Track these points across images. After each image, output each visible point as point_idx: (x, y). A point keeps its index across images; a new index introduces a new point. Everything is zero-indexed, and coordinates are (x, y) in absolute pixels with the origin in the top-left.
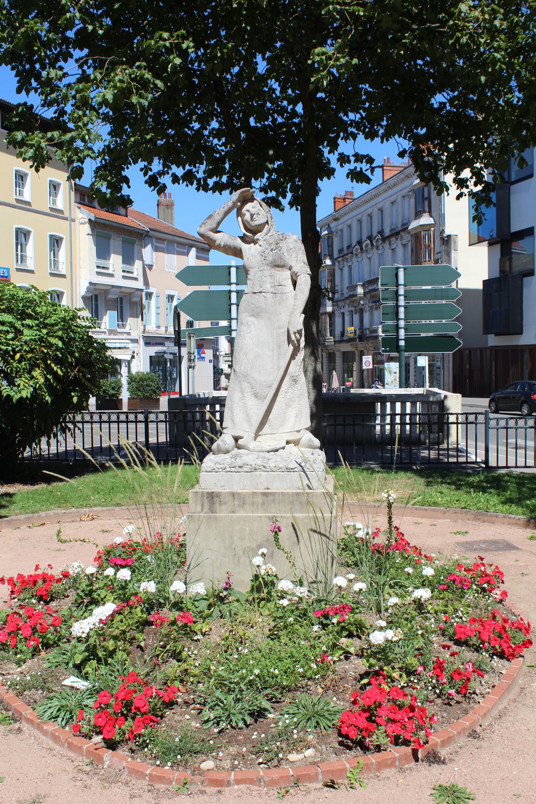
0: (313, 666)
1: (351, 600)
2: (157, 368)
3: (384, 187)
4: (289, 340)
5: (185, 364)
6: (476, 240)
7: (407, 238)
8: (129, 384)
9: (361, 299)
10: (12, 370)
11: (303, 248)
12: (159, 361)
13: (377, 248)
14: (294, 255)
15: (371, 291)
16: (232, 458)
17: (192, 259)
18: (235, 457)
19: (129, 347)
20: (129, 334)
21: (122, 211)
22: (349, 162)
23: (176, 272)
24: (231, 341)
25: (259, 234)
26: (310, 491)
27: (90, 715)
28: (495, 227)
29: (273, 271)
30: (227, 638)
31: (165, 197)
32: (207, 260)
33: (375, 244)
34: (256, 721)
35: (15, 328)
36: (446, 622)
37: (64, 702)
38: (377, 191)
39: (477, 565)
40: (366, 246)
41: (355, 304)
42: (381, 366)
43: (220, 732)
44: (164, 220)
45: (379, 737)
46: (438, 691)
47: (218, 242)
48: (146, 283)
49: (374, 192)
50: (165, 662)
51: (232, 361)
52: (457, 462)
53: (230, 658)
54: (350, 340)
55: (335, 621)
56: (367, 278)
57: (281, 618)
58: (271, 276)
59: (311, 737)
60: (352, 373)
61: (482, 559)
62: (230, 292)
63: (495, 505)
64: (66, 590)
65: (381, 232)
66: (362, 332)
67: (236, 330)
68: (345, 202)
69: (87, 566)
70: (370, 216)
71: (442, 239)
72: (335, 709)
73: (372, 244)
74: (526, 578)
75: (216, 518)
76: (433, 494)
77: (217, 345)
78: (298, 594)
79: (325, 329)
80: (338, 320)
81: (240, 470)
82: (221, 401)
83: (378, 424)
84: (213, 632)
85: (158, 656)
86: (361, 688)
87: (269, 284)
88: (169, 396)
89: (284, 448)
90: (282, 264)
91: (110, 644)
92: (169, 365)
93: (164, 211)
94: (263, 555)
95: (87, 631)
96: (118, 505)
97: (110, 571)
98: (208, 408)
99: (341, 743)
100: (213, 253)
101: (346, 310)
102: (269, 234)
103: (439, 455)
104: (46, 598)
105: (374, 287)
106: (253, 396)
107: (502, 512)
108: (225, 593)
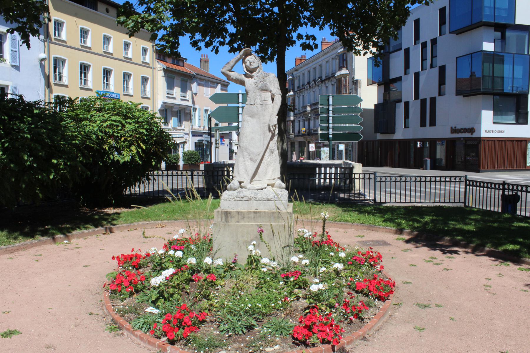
0: (280, 303)
1: (300, 269)
3: (322, 53)
4: (270, 130)
6: (371, 83)
7: (334, 81)
8: (183, 157)
9: (309, 113)
10: (120, 147)
13: (318, 86)
14: (273, 84)
17: (218, 90)
18: (239, 192)
19: (184, 136)
20: (183, 130)
21: (181, 64)
22: (302, 39)
24: (238, 134)
27: (160, 326)
28: (381, 76)
29: (261, 93)
30: (234, 288)
32: (227, 91)
34: (249, 331)
35: (122, 124)
36: (351, 281)
37: (146, 320)
39: (368, 252)
42: (319, 150)
43: (229, 336)
45: (314, 339)
46: (346, 317)
47: (232, 77)
48: (193, 103)
49: (317, 56)
50: (200, 300)
52: (359, 200)
53: (236, 298)
54: (303, 135)
55: (292, 279)
56: (312, 102)
57: (263, 278)
59: (278, 339)
61: (371, 248)
62: (238, 107)
63: (378, 222)
64: (148, 263)
65: (320, 77)
66: (309, 131)
69: (159, 250)
70: (315, 69)
71: (353, 82)
72: (291, 325)
73: (315, 84)
74: (394, 260)
76: (346, 216)
77: (231, 137)
78: (272, 265)
79: (290, 129)
80: (297, 124)
84: (227, 285)
85: (196, 297)
86: (305, 315)
89: (266, 188)
91: (171, 290)
94: (254, 245)
95: (159, 283)
96: (176, 219)
97: (171, 252)
99: (293, 343)
101: (301, 119)
103: (349, 196)
104: (137, 267)
105: (316, 107)
107: (382, 225)
108: (233, 265)
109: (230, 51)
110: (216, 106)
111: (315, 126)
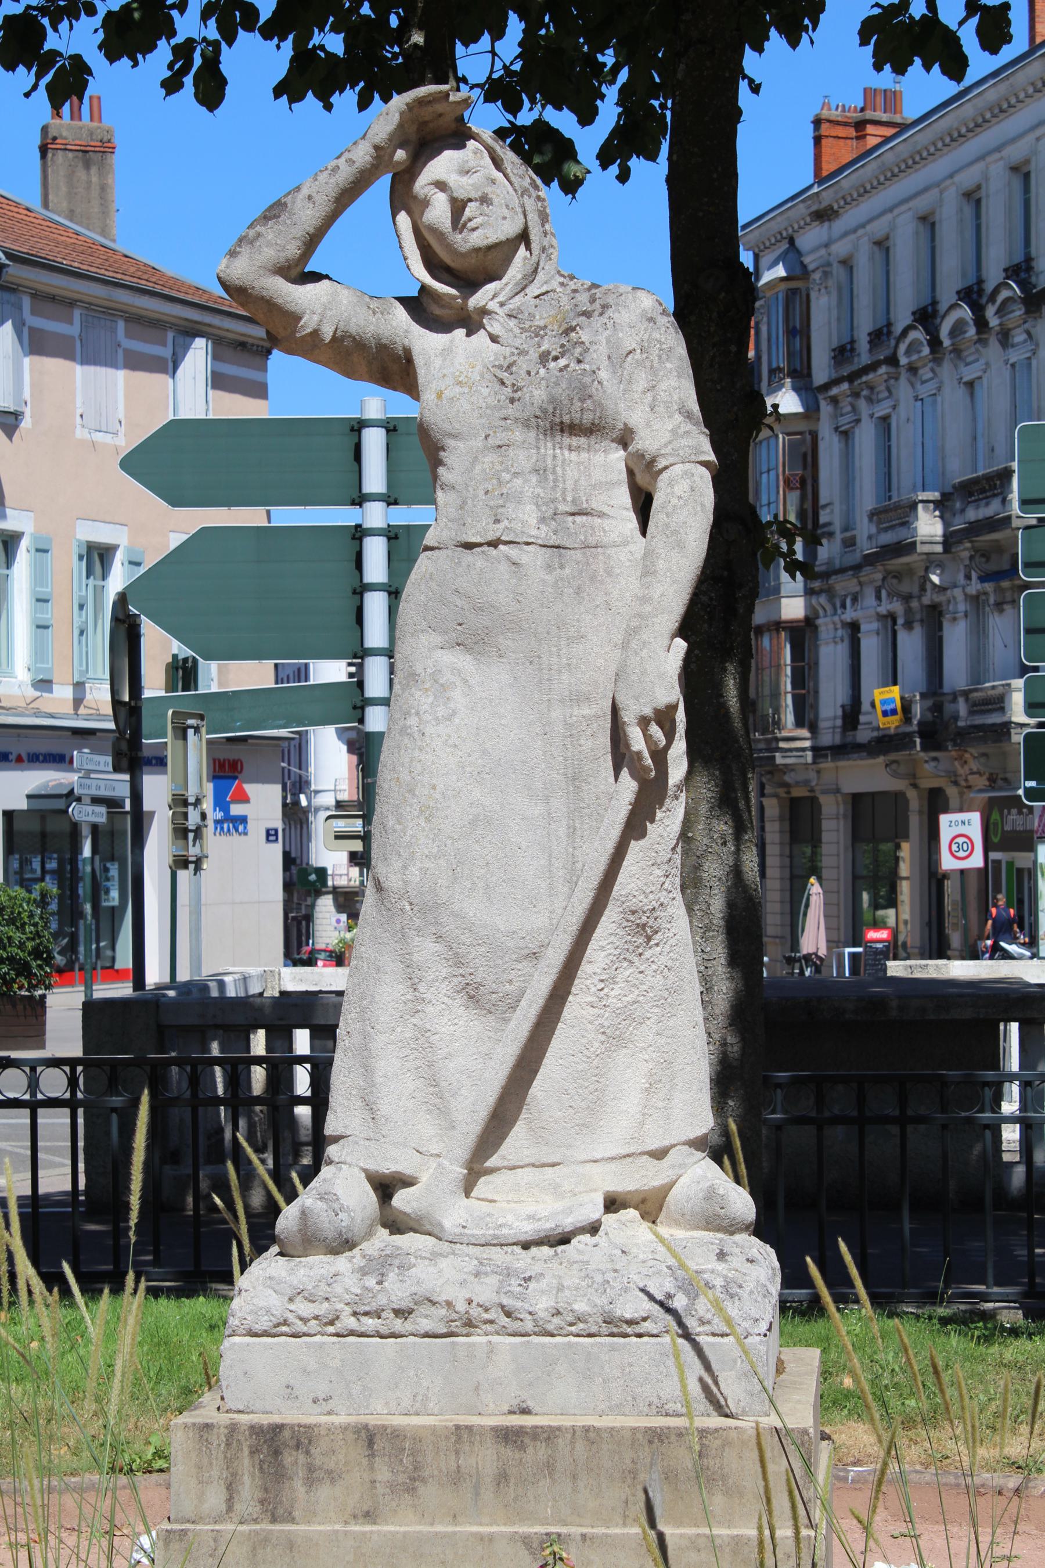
2: (36, 864)
4: (621, 755)
5: (157, 849)
9: (931, 562)
11: (681, 349)
12: (43, 835)
13: (1005, 338)
14: (641, 381)
15: (976, 528)
16: (363, 1272)
17: (191, 389)
23: (125, 442)
24: (365, 750)
25: (491, 287)
26: (716, 1421)
29: (548, 448)
31: (76, 115)
32: (259, 391)
33: (994, 322)
38: (1003, 88)
40: (954, 332)
42: (1022, 859)
44: (71, 215)
47: (308, 323)
51: (366, 838)
54: (885, 744)
56: (958, 472)
58: (540, 471)
60: (893, 889)
62: (359, 533)
66: (937, 708)
67: (385, 702)
68: (861, 137)
70: (973, 198)
73: (981, 324)
75: (291, 1545)
77: (302, 762)
79: (776, 695)
80: (831, 656)
81: (398, 1325)
82: (318, 1013)
83: (1011, 1120)
87: (530, 508)
88: (89, 990)
89: (594, 1229)
90: (587, 418)
92: (87, 852)
93: (70, 176)
101: (867, 612)
102: (534, 290)
105: (991, 509)
106: (461, 999)
109: (289, 89)
110: (172, 527)
111: (978, 669)
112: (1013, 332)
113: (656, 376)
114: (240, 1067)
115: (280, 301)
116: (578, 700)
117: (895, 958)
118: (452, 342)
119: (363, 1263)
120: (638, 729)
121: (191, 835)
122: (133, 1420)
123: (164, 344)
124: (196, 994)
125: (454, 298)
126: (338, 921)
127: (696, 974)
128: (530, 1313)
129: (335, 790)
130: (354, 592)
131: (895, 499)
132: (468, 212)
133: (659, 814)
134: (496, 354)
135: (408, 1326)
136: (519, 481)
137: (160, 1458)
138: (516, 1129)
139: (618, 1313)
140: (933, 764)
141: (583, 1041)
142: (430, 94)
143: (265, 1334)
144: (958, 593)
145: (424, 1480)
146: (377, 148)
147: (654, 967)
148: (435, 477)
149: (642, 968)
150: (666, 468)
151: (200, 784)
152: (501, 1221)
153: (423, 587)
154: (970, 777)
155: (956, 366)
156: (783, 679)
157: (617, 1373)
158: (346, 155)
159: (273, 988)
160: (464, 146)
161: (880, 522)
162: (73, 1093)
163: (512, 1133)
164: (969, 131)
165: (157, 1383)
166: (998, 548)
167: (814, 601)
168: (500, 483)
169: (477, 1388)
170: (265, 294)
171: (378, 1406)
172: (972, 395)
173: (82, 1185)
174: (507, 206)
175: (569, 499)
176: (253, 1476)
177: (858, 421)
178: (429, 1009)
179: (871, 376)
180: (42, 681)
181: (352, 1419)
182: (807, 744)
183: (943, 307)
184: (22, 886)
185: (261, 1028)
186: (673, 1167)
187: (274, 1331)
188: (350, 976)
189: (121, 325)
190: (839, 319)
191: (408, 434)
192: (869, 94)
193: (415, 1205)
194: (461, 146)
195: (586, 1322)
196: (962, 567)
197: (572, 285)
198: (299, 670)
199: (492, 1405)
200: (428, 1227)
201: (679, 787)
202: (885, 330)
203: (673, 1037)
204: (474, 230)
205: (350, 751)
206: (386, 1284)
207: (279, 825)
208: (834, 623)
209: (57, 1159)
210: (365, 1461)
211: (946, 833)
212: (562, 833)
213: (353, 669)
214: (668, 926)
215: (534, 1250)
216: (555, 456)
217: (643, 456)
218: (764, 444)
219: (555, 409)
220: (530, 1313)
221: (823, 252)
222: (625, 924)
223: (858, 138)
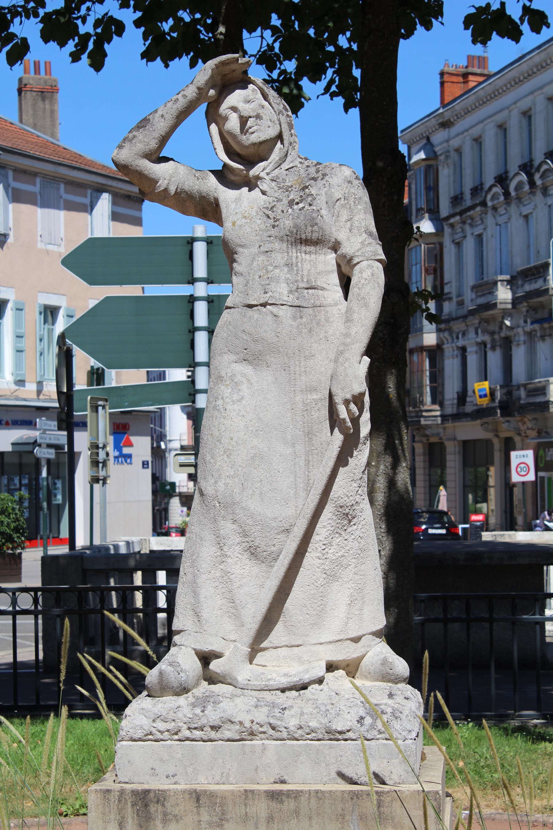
2: (17, 481)
4: (334, 420)
9: (505, 313)
11: (366, 198)
12: (21, 465)
15: (529, 295)
16: (194, 705)
17: (101, 221)
18: (202, 703)
23: (64, 250)
24: (195, 417)
25: (262, 165)
29: (294, 253)
32: (138, 222)
33: (539, 182)
38: (543, 55)
40: (517, 188)
41: (492, 327)
44: (35, 127)
47: (162, 185)
49: (537, 58)
51: (195, 466)
54: (480, 413)
56: (520, 264)
62: (192, 299)
66: (509, 393)
67: (205, 391)
68: (466, 82)
70: (527, 115)
73: (532, 183)
77: (162, 424)
79: (421, 387)
80: (451, 365)
81: (213, 734)
87: (284, 285)
88: (45, 550)
89: (320, 681)
90: (315, 236)
92: (44, 474)
93: (34, 105)
98: (138, 579)
100: (150, 209)
101: (470, 341)
102: (285, 166)
105: (538, 284)
106: (247, 555)
110: (92, 296)
111: (531, 373)
112: (550, 188)
113: (353, 213)
114: (127, 592)
115: (146, 172)
116: (310, 391)
117: (487, 530)
118: (240, 194)
119: (193, 700)
120: (343, 406)
121: (101, 465)
122: (69, 787)
123: (85, 196)
124: (103, 552)
125: (241, 170)
126: (182, 511)
127: (376, 540)
128: (286, 728)
129: (180, 440)
130: (190, 332)
131: (485, 279)
132: (249, 124)
133: (355, 453)
134: (264, 201)
135: (218, 735)
136: (277, 271)
137: (83, 807)
138: (277, 626)
139: (334, 727)
140: (507, 424)
141: (314, 577)
142: (228, 59)
143: (140, 740)
144: (520, 330)
145: (227, 820)
146: (199, 88)
147: (353, 537)
148: (232, 269)
149: (346, 537)
150: (358, 263)
151: (106, 438)
152: (269, 677)
153: (225, 329)
154: (528, 431)
155: (518, 207)
156: (425, 377)
157: (333, 761)
158: (182, 93)
159: (146, 548)
160: (247, 88)
161: (477, 292)
162: (36, 607)
163: (275, 629)
164: (525, 78)
165: (82, 766)
166: (542, 306)
167: (441, 335)
168: (267, 272)
169: (256, 769)
170: (138, 169)
171: (202, 779)
172: (527, 222)
173: (41, 656)
174: (270, 120)
175: (305, 280)
176: (133, 818)
177: (465, 237)
178: (229, 560)
179: (472, 212)
180: (20, 381)
181: (188, 787)
182: (438, 413)
183: (511, 174)
184: (8, 493)
185: (139, 570)
186: (364, 647)
187: (145, 738)
188: (186, 542)
189: (62, 186)
190: (454, 181)
191: (218, 245)
192: (470, 58)
193: (222, 668)
194: (245, 87)
195: (316, 732)
196: (522, 317)
197: (306, 163)
198: (160, 374)
199: (265, 779)
200: (230, 681)
201: (366, 438)
202: (479, 187)
203: (363, 575)
204: (252, 133)
205: (189, 417)
206: (206, 712)
207: (149, 459)
208: (453, 347)
209: (28, 643)
210: (195, 810)
211: (514, 462)
212: (302, 463)
213: (190, 374)
214: (361, 514)
215: (288, 693)
216: (297, 257)
217: (345, 256)
218: (414, 250)
219: (297, 231)
220: (286, 728)
221: (445, 145)
222: (337, 513)
223: (464, 82)
